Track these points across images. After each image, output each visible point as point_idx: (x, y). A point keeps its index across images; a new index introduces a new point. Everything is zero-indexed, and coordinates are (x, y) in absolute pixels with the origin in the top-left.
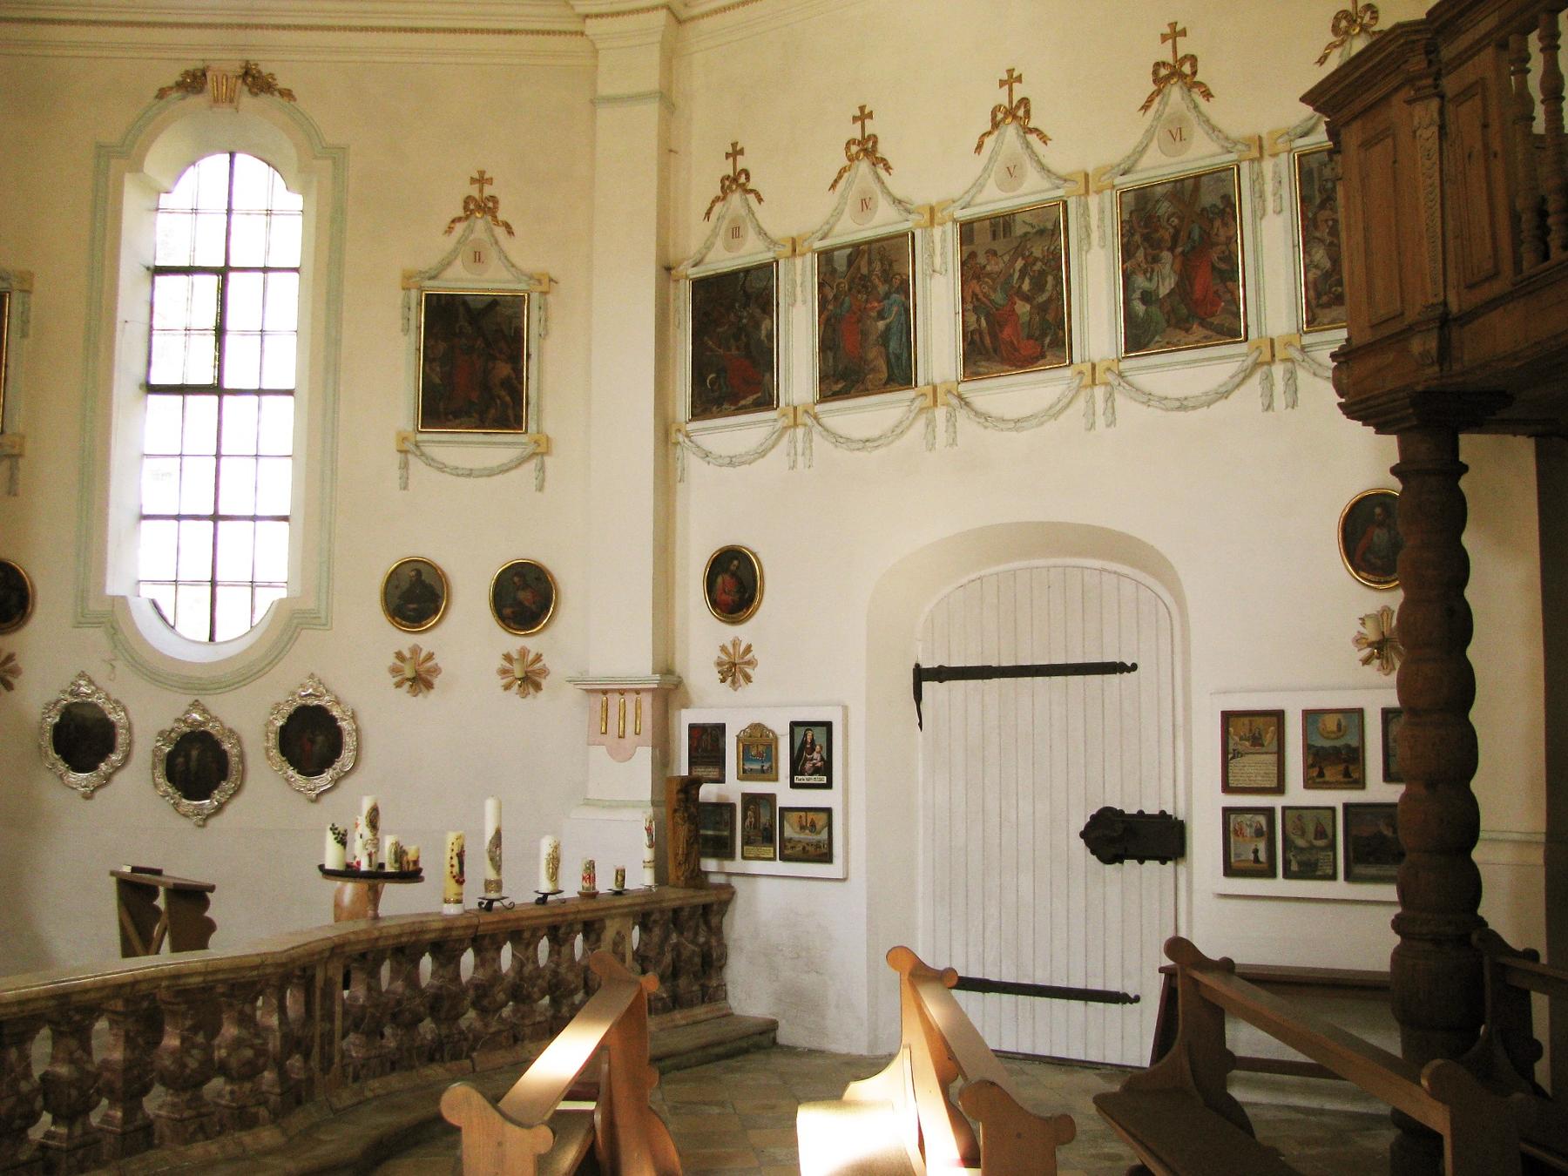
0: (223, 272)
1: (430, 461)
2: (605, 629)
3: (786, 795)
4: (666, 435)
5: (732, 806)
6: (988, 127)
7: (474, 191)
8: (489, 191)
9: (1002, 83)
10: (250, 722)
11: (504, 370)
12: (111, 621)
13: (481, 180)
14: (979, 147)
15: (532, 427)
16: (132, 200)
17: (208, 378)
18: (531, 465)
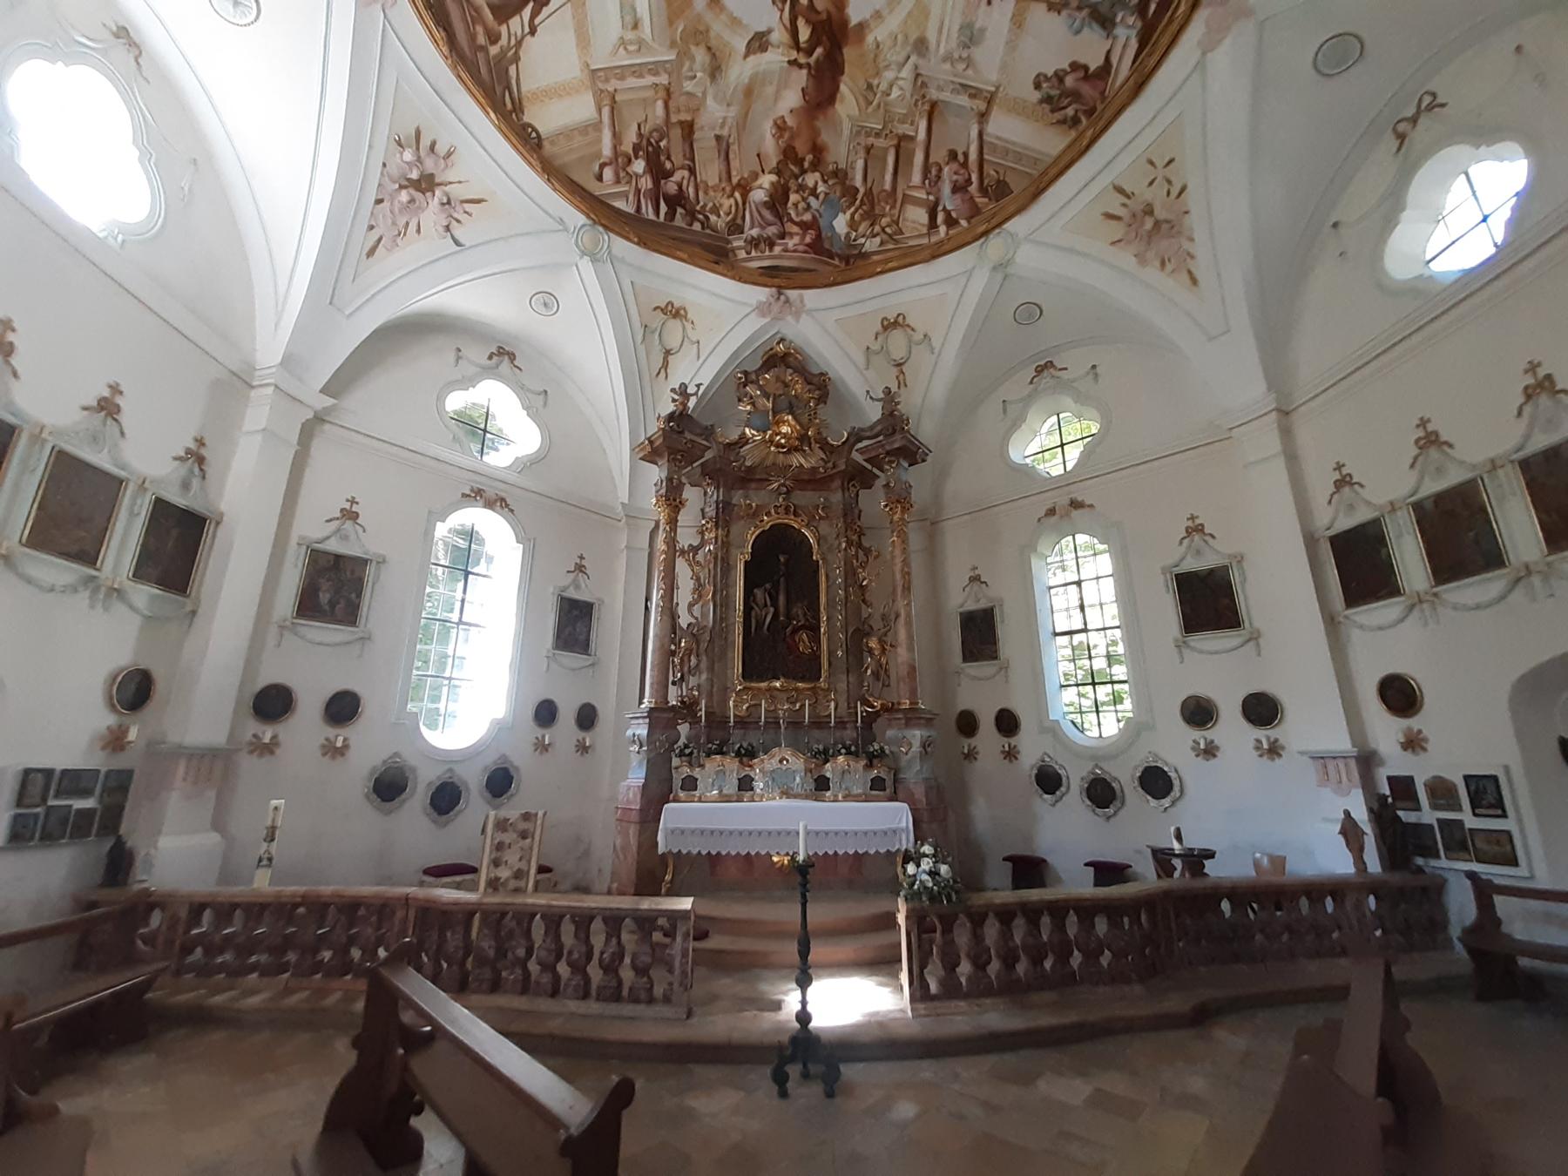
0: (1079, 583)
1: (1193, 649)
2: (1314, 723)
3: (1470, 821)
4: (1332, 623)
5: (1431, 826)
6: (1522, 399)
8: (1198, 522)
9: (1526, 372)
10: (1125, 776)
11: (1226, 601)
12: (1054, 730)
13: (582, 558)
14: (1520, 414)
15: (1247, 624)
16: (1035, 563)
17: (1080, 626)
18: (1251, 644)
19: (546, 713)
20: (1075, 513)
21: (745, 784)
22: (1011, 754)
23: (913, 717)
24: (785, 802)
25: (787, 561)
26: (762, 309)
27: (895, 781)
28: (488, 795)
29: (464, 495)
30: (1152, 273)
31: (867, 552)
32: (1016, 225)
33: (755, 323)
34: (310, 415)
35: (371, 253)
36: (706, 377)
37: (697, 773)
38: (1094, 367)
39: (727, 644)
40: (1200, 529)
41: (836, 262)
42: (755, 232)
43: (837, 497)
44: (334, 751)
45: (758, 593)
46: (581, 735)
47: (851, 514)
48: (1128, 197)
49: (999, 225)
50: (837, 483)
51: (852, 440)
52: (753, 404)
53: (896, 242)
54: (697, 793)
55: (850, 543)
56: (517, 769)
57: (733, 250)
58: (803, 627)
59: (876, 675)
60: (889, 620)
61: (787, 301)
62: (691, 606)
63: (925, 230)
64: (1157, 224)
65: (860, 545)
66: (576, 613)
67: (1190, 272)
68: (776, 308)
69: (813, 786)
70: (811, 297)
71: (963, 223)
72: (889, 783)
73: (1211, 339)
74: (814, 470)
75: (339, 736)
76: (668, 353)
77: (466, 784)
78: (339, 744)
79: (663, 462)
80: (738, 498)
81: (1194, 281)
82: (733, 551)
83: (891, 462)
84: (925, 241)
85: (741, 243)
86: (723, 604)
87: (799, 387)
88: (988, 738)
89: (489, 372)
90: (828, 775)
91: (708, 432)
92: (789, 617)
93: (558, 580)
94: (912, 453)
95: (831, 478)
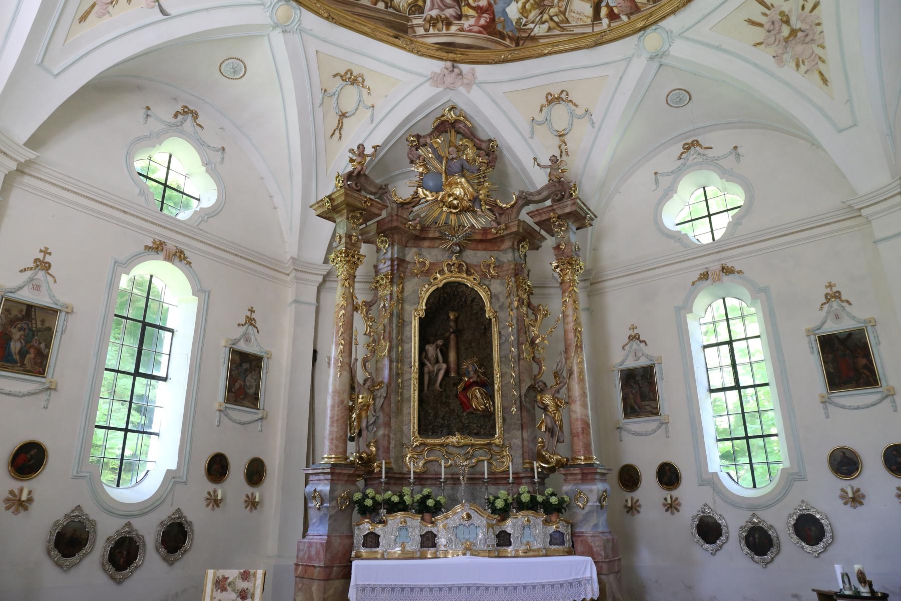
1: (837, 405)
7: (248, 314)
11: (863, 361)
13: (252, 311)
15: (884, 383)
19: (217, 467)
20: (725, 278)
21: (429, 540)
22: (672, 506)
23: (588, 473)
24: (468, 558)
25: (456, 320)
26: (436, 79)
27: (573, 535)
28: (163, 550)
29: (147, 247)
30: (788, 71)
31: (535, 310)
32: (670, 23)
33: (428, 92)
34: (13, 166)
35: (83, 18)
36: (379, 138)
37: (379, 529)
38: (736, 148)
39: (403, 400)
40: (837, 295)
41: (507, 42)
42: (434, 13)
43: (507, 257)
44: (19, 504)
45: (431, 349)
46: (249, 490)
47: (519, 271)
48: (769, 9)
49: (655, 22)
50: (507, 244)
51: (520, 202)
52: (425, 166)
53: (563, 29)
54: (380, 550)
55: (521, 302)
56: (190, 524)
57: (412, 27)
58: (475, 383)
59: (551, 431)
60: (562, 377)
61: (461, 74)
62: (365, 361)
63: (589, 21)
64: (794, 32)
65: (529, 305)
66: (246, 366)
67: (821, 74)
68: (450, 79)
69: (494, 542)
70: (482, 71)
71: (624, 18)
72: (568, 537)
73: (840, 131)
74: (485, 230)
75: (27, 486)
76: (343, 115)
77: (141, 537)
78: (24, 497)
79: (342, 220)
80: (411, 255)
81: (825, 81)
82: (407, 307)
83: (560, 226)
84: (589, 30)
85: (420, 21)
86: (399, 360)
87: (470, 152)
88: (649, 489)
89: (174, 129)
90: (509, 530)
91: (383, 191)
92: (458, 372)
93: (228, 332)
94: (580, 218)
95: (502, 239)
